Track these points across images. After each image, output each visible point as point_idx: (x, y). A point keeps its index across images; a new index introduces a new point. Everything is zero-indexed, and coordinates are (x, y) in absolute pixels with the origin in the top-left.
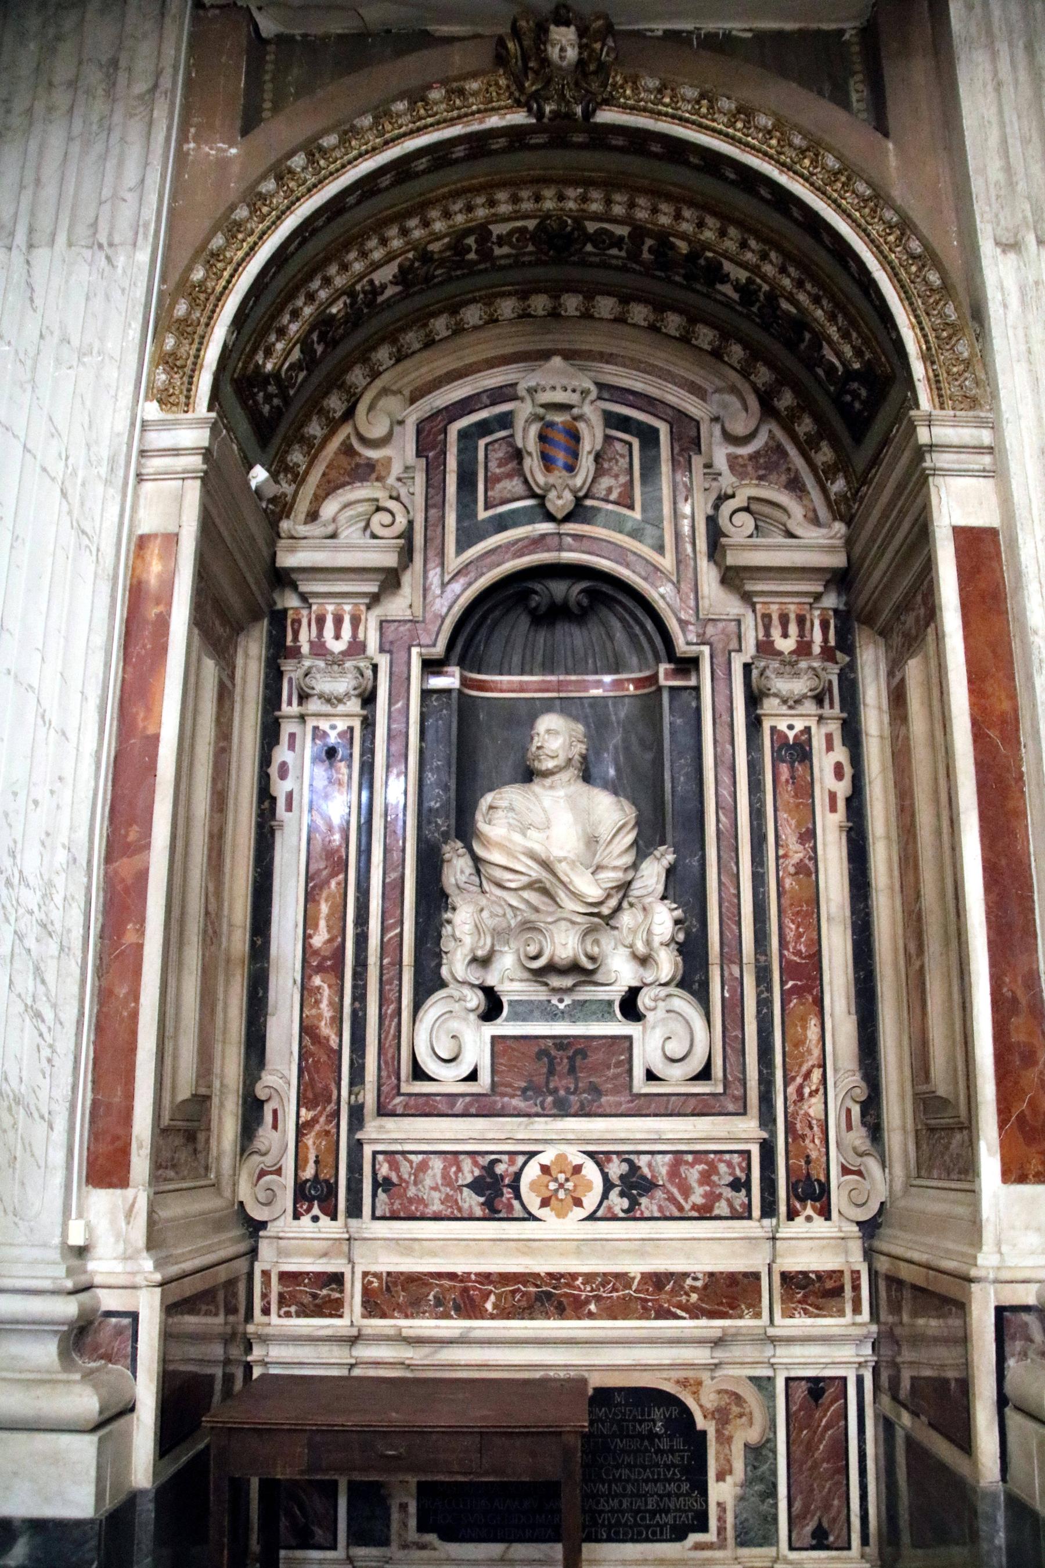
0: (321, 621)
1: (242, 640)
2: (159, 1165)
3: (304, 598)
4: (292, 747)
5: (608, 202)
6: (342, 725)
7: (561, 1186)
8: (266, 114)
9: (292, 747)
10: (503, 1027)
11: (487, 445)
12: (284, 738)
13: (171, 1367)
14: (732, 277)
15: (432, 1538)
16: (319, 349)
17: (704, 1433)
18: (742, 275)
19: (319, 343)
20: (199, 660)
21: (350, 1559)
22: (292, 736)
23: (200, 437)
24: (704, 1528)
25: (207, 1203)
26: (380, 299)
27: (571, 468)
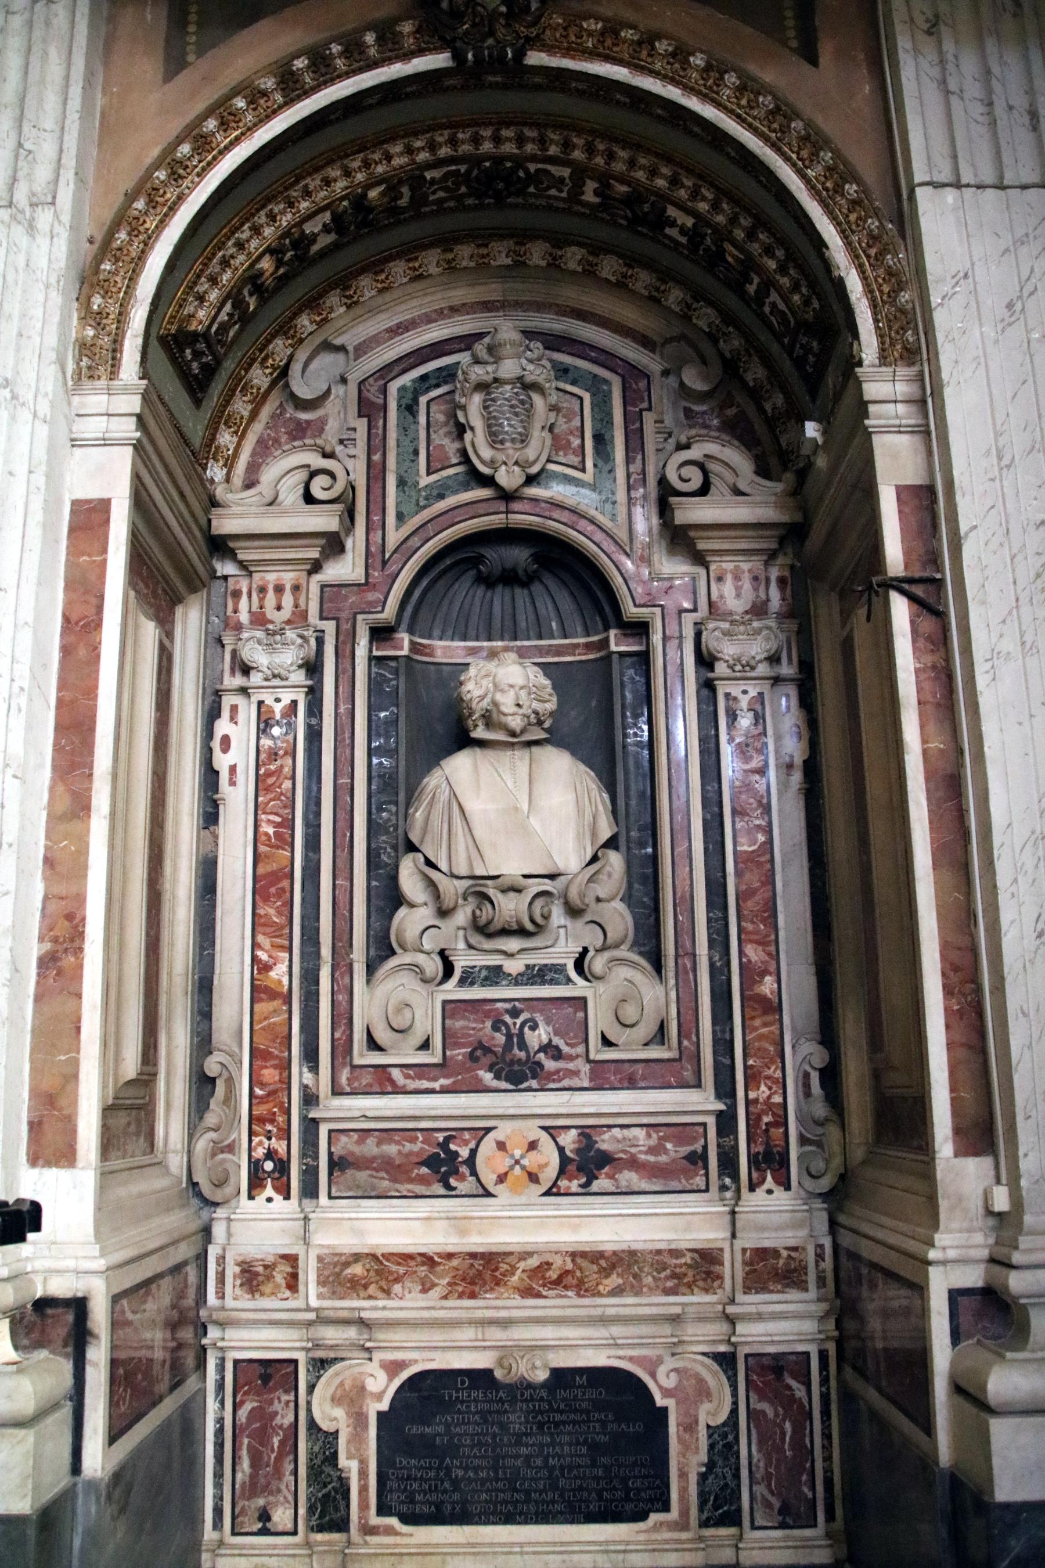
0: (262, 590)
1: (179, 611)
2: (108, 1145)
3: (243, 565)
4: (233, 719)
5: (542, 142)
6: (287, 698)
7: (517, 1162)
8: (191, 58)
9: (233, 719)
10: (451, 990)
11: (428, 403)
12: (226, 713)
13: (123, 1355)
14: (679, 222)
15: (393, 1521)
16: (252, 303)
17: (665, 1409)
18: (690, 222)
19: (251, 295)
20: (137, 627)
21: (308, 1544)
22: (234, 709)
23: (134, 403)
24: (666, 1508)
25: (154, 1183)
26: (315, 248)
27: (524, 439)
